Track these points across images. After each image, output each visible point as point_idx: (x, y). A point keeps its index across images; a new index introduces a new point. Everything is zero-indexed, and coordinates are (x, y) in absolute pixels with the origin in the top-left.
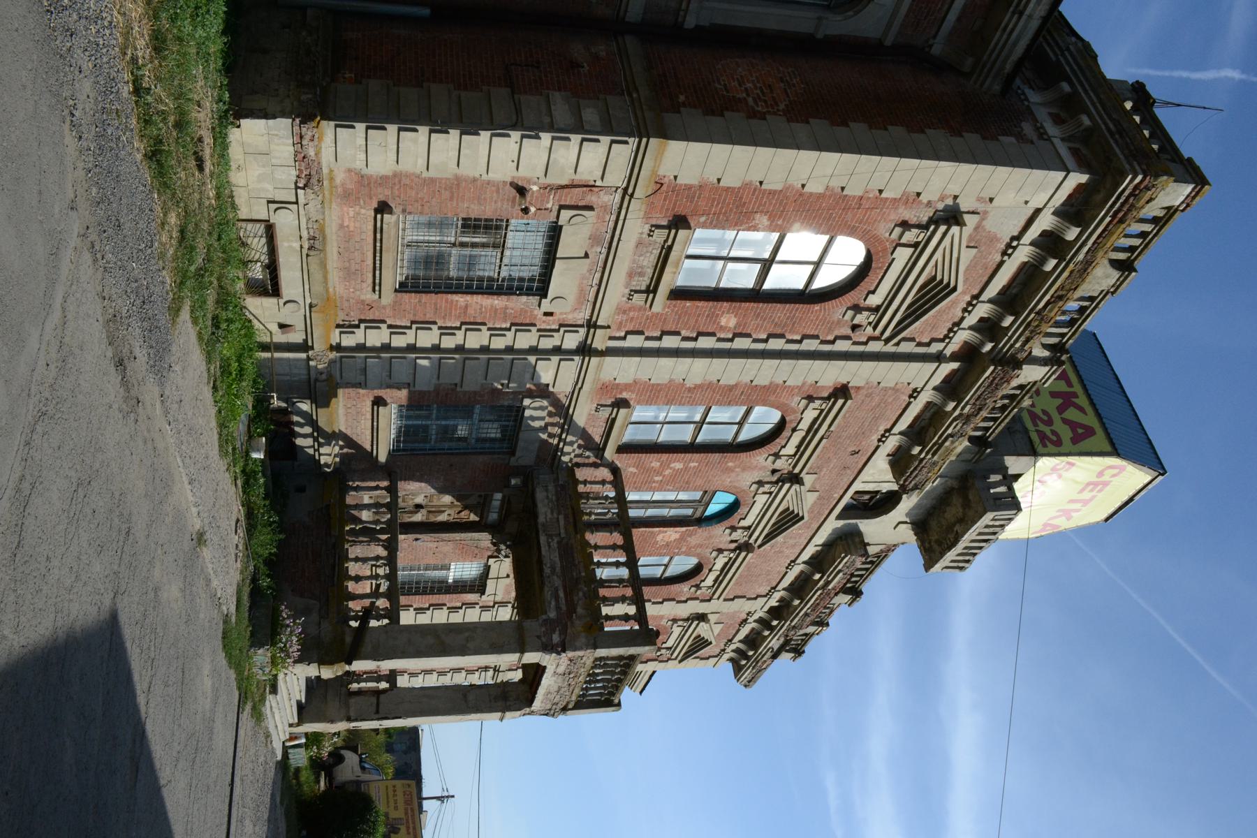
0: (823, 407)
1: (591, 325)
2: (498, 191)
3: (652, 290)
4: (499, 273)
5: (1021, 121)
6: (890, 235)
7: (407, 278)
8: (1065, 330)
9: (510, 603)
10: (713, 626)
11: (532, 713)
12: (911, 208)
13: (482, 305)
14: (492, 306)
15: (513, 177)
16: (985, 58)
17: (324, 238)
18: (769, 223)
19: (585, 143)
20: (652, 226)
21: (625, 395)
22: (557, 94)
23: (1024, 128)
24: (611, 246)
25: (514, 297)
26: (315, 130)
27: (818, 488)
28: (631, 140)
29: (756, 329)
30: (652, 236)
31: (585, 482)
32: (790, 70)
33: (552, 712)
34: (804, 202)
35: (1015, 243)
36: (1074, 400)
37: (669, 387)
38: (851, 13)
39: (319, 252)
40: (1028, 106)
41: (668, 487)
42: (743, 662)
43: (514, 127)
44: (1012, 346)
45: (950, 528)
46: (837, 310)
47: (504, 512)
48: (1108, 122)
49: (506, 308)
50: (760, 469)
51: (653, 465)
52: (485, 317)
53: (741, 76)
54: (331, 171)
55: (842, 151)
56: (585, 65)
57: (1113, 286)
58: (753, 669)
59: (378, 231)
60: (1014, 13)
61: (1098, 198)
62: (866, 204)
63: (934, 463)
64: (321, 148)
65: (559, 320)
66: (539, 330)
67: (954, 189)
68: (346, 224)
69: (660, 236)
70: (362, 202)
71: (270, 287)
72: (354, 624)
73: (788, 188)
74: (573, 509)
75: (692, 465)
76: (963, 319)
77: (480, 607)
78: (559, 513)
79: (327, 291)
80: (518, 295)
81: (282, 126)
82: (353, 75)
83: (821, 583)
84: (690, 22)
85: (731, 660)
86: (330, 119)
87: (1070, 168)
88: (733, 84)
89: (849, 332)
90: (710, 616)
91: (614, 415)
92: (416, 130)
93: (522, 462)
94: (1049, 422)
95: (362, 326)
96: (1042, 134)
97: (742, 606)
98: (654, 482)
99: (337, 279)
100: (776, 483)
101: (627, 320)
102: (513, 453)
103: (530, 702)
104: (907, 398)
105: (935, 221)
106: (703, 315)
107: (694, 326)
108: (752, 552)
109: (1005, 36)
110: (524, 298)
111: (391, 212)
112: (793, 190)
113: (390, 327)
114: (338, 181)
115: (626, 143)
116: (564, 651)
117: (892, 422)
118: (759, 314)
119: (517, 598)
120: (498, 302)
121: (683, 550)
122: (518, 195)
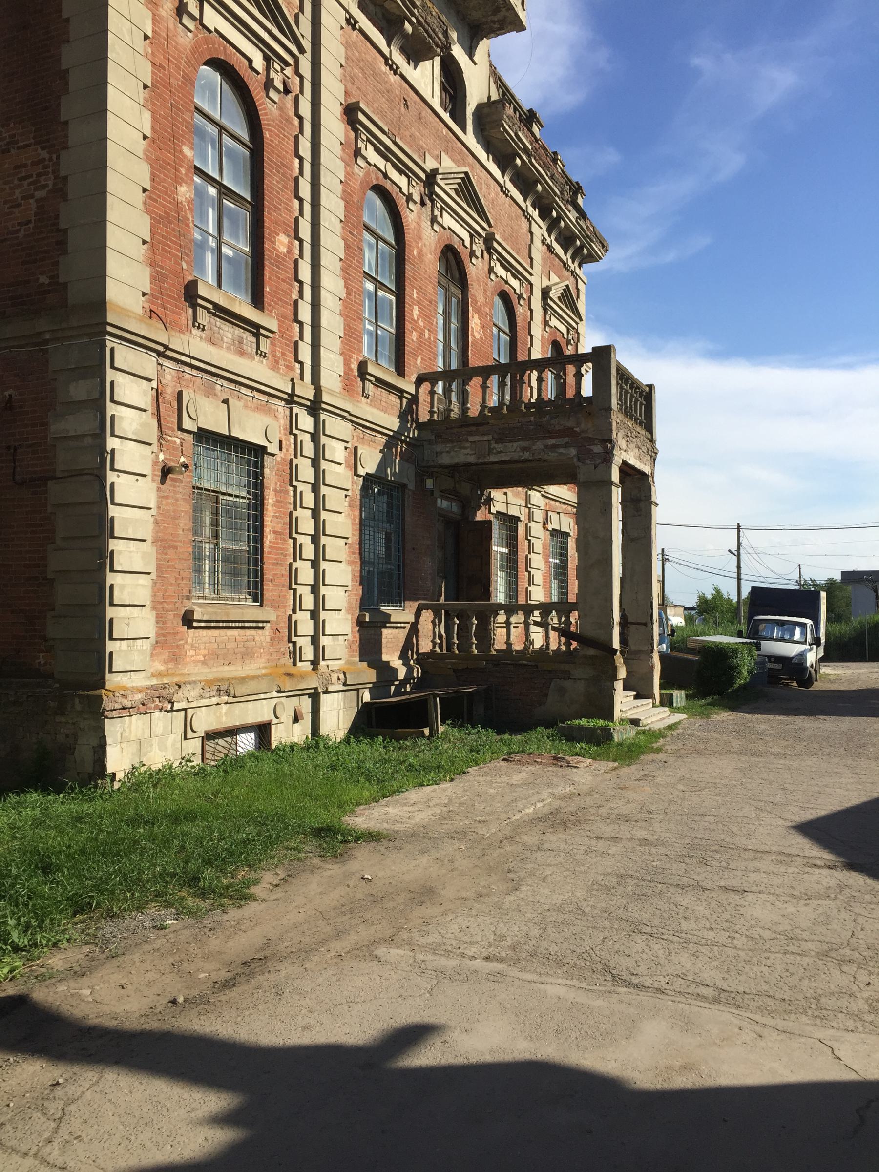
0: (364, 138)
1: (291, 399)
2: (167, 497)
3: (256, 329)
4: (243, 498)
6: (191, 31)
9: (527, 492)
10: (552, 282)
13: (274, 516)
14: (274, 505)
15: (153, 480)
17: (219, 680)
18: (184, 184)
20: (194, 326)
21: (354, 366)
22: (53, 428)
24: (214, 373)
25: (265, 481)
26: (117, 694)
27: (437, 153)
28: (109, 345)
29: (289, 211)
30: (204, 326)
31: (431, 412)
33: (653, 454)
34: (161, 139)
37: (347, 316)
39: (231, 685)
41: (434, 323)
42: (585, 251)
43: (101, 478)
47: (451, 496)
49: (275, 490)
50: (420, 218)
51: (415, 339)
52: (284, 513)
54: (153, 675)
55: (105, 82)
56: (7, 393)
58: (592, 241)
59: (210, 625)
62: (160, 59)
63: (423, 7)
65: (286, 434)
66: (296, 457)
68: (202, 659)
69: (204, 318)
70: (181, 642)
71: (263, 731)
72: (574, 644)
73: (147, 157)
74: (461, 426)
75: (415, 295)
77: (530, 522)
78: (467, 441)
79: (265, 675)
80: (263, 477)
81: (113, 729)
82: (41, 655)
85: (580, 266)
86: (104, 678)
89: (290, 97)
90: (544, 285)
91: (373, 379)
92: (112, 586)
95: (294, 639)
98: (430, 339)
99: (252, 666)
100: (432, 201)
101: (285, 360)
102: (404, 486)
104: (356, 32)
106: (276, 272)
108: (494, 234)
110: (267, 471)
112: (149, 152)
113: (294, 611)
114: (161, 668)
115: (112, 350)
116: (611, 441)
118: (275, 206)
119: (524, 487)
120: (270, 499)
121: (487, 310)
122: (170, 475)
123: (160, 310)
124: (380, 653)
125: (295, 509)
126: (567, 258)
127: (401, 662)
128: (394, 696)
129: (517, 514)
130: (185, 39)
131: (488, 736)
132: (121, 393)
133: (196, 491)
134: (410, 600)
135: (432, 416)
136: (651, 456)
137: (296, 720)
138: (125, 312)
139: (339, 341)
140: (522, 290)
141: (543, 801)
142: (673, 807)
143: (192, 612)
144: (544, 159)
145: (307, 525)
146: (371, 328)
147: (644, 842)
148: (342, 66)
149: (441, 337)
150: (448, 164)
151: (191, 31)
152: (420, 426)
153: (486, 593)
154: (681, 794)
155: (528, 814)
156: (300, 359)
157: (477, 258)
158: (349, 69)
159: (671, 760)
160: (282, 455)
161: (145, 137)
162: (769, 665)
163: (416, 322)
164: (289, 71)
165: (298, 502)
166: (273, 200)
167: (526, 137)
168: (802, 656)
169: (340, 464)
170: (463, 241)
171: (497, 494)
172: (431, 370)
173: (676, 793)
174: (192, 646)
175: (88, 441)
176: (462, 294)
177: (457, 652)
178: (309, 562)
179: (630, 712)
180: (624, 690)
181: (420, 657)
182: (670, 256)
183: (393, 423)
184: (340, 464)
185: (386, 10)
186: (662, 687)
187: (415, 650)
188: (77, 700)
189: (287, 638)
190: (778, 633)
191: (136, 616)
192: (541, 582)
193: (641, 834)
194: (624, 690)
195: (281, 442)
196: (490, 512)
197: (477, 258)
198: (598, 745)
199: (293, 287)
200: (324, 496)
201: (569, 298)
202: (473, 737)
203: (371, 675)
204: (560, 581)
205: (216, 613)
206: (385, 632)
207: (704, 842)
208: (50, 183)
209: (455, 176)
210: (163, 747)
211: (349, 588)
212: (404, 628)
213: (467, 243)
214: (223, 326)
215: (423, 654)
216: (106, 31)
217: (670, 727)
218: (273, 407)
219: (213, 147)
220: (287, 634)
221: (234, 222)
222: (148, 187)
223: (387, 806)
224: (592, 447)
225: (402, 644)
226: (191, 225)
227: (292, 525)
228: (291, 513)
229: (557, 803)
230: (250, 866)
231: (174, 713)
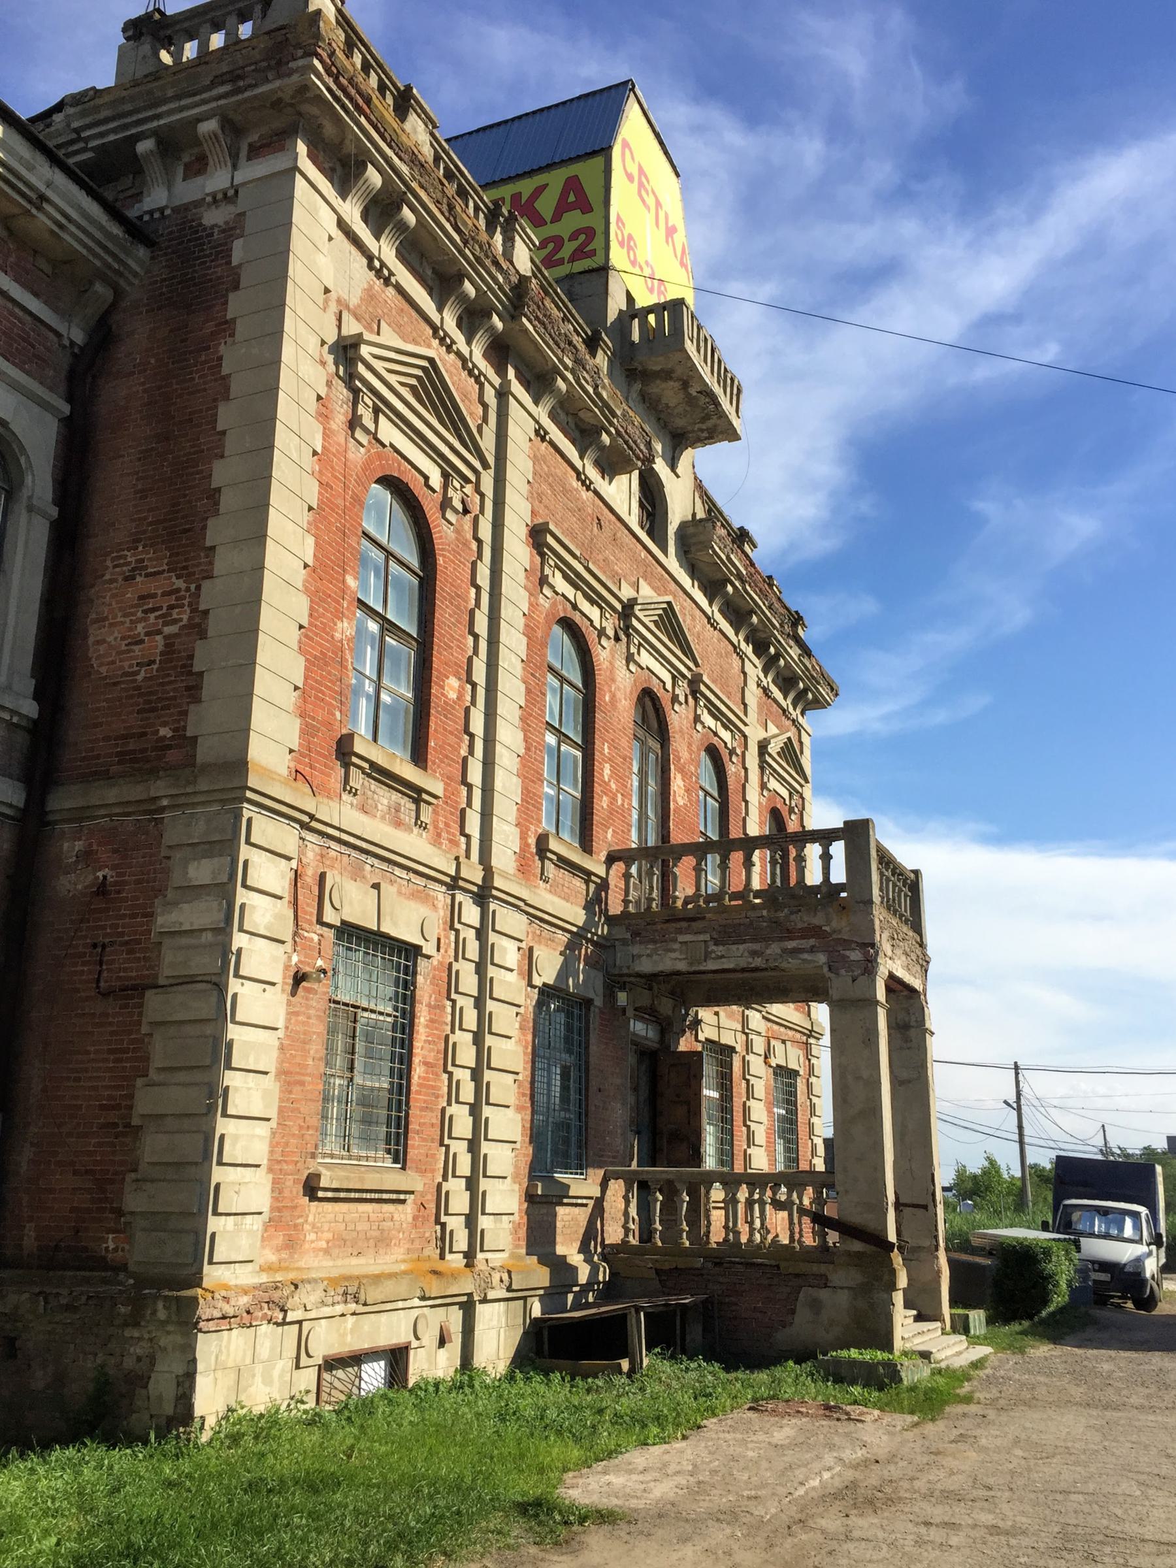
0: (552, 563)
1: (454, 883)
2: (296, 1014)
3: (416, 794)
4: (389, 1015)
5: (201, 225)
6: (363, 446)
7: (388, 1152)
8: (471, 204)
10: (770, 734)
11: (925, 990)
12: (332, 412)
13: (425, 1041)
14: (427, 1026)
15: (283, 991)
16: (98, 263)
19: (249, 883)
21: (532, 841)
22: (160, 920)
23: (212, 222)
25: (418, 992)
26: (217, 1296)
28: (246, 814)
31: (626, 902)
32: (109, 563)
35: (377, 264)
36: (523, 201)
37: (526, 778)
38: (23, 460)
40: (173, 210)
42: (810, 696)
43: (220, 988)
44: (501, 288)
45: (690, 401)
46: (444, 531)
48: (215, 92)
49: (429, 1005)
50: (613, 657)
51: (605, 806)
53: (123, 638)
54: (262, 1269)
55: (267, 505)
56: (100, 874)
57: (426, 126)
58: (819, 683)
59: (341, 1196)
60: (39, 209)
61: (329, 130)
63: (624, 416)
64: (236, 1286)
66: (456, 960)
67: (313, 344)
69: (357, 779)
70: (300, 1220)
71: (397, 1358)
73: (306, 588)
74: (668, 921)
75: (606, 750)
76: (459, 354)
79: (405, 1273)
80: (415, 987)
81: (207, 1348)
82: (111, 1236)
83: (737, 583)
84: (30, 709)
85: (803, 714)
87: (290, 165)
88: (137, 653)
91: (554, 857)
92: (222, 1137)
93: (600, 989)
94: (558, 241)
96: (229, 197)
97: (753, 695)
99: (389, 1258)
100: (628, 636)
101: (448, 832)
102: (588, 1002)
103: (912, 991)
105: (350, 378)
106: (444, 723)
107: (456, 736)
108: (701, 675)
109: (73, 229)
110: (420, 979)
111: (318, 1176)
113: (445, 1178)
115: (250, 820)
116: (873, 945)
117: (569, 469)
118: (445, 643)
119: (737, 1002)
121: (693, 769)
122: (304, 984)
123: (306, 770)
124: (553, 1243)
125: (453, 1032)
126: (787, 703)
127: (581, 1257)
128: (573, 1309)
129: (731, 1043)
130: (357, 455)
131: (710, 1373)
132: (256, 876)
133: (332, 1005)
134: (594, 1167)
135: (626, 906)
136: (922, 966)
137: (442, 1342)
138: (267, 773)
139: (515, 808)
140: (735, 744)
141: (829, 1469)
142: (1021, 1482)
143: (318, 1176)
144: (760, 585)
145: (467, 1055)
146: (552, 792)
147: (994, 1530)
148: (529, 482)
149: (635, 803)
150: (646, 592)
151: (363, 446)
152: (611, 920)
153: (696, 1157)
154: (1023, 1462)
155: (814, 1488)
156: (467, 831)
157: (681, 704)
158: (536, 485)
159: (991, 1414)
160: (440, 958)
161: (306, 566)
162: (1095, 1276)
163: (607, 784)
164: (469, 489)
165: (456, 1023)
166: (444, 636)
167: (740, 560)
168: (1139, 1261)
169: (512, 970)
170: (664, 683)
171: (705, 1014)
172: (624, 847)
173: (1015, 1461)
174: (314, 1226)
175: (208, 937)
176: (662, 747)
177: (660, 1244)
178: (467, 1107)
179: (917, 1340)
180: (905, 1307)
181: (607, 1250)
182: (940, 717)
183: (577, 915)
184: (512, 970)
185: (581, 420)
186: (953, 1303)
187: (599, 1240)
188: (160, 1305)
189: (433, 1218)
190: (1100, 1226)
191: (246, 1180)
192: (763, 1142)
193: (987, 1518)
194: (905, 1307)
195: (439, 939)
196: (697, 1040)
197: (681, 704)
198: (881, 1389)
199: (461, 740)
200: (491, 1013)
201: (790, 753)
202: (693, 1375)
203: (542, 1277)
204: (788, 1141)
205: (348, 1178)
206: (561, 1211)
207: (1080, 1531)
208: (185, 617)
209: (656, 606)
210: (267, 1381)
211: (518, 1146)
212: (585, 1205)
213: (669, 686)
214: (378, 790)
215: (612, 1246)
216: (271, 447)
217: (977, 1365)
218: (432, 893)
219: (377, 575)
220: (434, 1211)
221: (396, 663)
222: (305, 623)
223: (605, 1473)
224: (847, 953)
225: (582, 1231)
226: (350, 667)
227: (448, 1053)
228: (447, 1037)
229: (850, 1475)
230: (445, 1554)
231: (286, 1327)
